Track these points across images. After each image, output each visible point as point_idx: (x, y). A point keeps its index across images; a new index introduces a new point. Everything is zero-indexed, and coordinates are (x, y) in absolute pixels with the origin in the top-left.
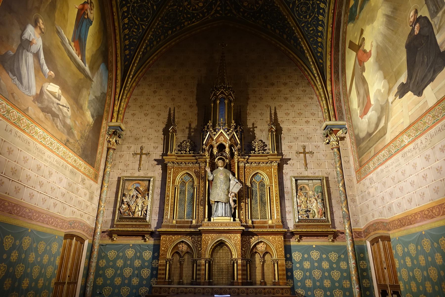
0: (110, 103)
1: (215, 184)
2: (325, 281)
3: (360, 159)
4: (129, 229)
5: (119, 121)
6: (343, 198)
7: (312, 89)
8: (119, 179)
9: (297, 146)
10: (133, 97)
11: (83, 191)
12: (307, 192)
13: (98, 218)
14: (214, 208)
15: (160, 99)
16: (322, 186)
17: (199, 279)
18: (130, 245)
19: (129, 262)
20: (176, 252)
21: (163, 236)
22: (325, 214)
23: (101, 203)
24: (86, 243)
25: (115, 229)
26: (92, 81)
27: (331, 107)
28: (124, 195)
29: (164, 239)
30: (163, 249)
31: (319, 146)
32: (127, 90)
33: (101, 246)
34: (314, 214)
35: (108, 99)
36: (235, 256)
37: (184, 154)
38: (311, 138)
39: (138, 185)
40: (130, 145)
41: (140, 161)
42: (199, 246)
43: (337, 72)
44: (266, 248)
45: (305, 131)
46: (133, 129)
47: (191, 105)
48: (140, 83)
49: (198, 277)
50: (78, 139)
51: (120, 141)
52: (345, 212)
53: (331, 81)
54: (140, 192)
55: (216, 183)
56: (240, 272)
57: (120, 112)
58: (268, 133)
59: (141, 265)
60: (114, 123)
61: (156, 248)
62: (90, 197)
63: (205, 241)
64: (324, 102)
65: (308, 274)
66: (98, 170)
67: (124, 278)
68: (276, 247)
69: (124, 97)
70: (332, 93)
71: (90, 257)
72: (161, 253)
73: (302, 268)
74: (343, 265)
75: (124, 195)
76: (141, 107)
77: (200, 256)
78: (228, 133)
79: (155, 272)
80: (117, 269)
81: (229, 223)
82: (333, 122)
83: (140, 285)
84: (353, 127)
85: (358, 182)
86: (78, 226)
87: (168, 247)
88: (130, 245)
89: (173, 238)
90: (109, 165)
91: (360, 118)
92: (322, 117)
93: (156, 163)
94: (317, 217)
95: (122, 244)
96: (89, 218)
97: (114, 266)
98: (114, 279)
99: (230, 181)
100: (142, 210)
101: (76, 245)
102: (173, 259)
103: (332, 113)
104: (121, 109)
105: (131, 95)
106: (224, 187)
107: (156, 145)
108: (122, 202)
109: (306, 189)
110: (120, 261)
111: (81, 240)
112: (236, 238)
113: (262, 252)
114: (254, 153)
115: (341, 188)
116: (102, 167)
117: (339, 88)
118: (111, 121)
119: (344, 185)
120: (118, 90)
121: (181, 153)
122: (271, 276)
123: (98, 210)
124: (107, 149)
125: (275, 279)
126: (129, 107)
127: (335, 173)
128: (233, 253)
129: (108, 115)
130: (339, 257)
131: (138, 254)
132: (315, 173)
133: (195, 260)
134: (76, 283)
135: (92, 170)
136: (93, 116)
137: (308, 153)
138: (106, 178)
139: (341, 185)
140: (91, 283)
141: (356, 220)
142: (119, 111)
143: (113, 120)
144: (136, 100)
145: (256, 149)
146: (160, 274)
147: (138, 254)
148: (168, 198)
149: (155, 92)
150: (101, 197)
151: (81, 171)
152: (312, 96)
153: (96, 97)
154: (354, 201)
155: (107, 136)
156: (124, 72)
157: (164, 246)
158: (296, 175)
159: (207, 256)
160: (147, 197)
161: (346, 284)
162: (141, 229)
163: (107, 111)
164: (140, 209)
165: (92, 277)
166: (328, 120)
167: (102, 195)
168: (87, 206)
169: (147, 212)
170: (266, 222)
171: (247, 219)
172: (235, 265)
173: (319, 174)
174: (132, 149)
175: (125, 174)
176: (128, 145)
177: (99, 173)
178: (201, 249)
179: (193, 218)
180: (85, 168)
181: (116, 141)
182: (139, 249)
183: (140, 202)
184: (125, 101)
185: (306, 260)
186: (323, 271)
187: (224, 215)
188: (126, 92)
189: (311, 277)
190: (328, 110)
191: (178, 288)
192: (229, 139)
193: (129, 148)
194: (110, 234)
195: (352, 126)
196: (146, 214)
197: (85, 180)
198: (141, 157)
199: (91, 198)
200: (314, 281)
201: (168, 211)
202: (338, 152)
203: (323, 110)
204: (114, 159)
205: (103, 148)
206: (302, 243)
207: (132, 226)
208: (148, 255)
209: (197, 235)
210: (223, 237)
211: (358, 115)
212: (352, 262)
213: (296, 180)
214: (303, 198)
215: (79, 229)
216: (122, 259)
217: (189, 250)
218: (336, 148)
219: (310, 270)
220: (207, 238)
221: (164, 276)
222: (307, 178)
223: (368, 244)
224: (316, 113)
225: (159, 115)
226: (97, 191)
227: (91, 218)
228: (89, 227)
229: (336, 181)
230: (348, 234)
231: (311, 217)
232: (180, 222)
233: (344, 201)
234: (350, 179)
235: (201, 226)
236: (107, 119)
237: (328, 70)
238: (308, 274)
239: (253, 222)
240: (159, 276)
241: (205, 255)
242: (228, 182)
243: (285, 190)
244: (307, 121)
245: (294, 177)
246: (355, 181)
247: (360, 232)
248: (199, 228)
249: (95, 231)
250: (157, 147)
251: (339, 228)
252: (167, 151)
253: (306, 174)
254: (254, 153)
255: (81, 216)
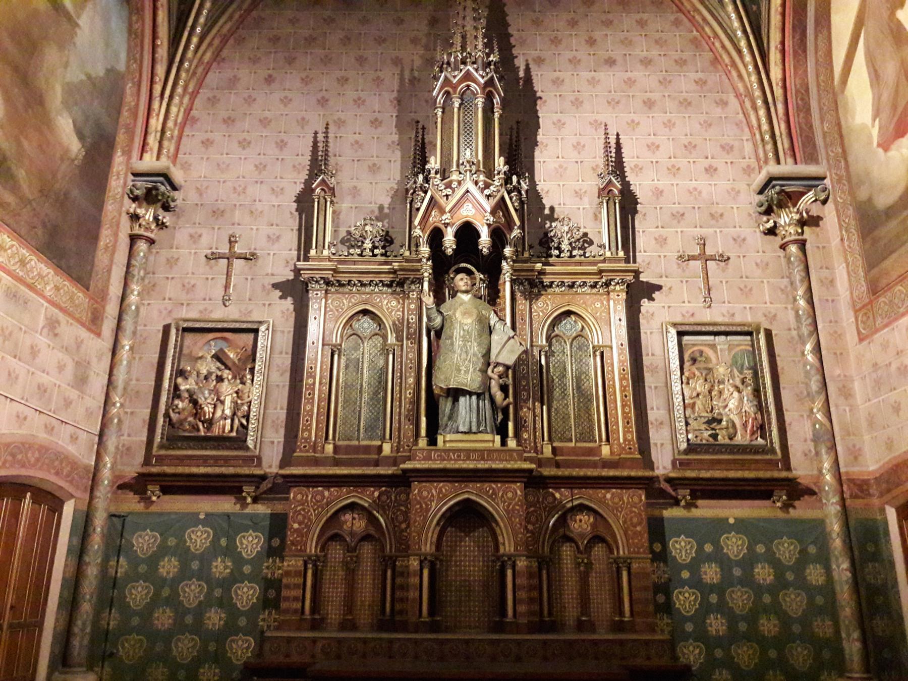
0: (137, 105)
1: (448, 342)
2: (763, 621)
3: (875, 271)
4: (195, 470)
5: (164, 159)
6: (815, 386)
7: (724, 77)
8: (166, 329)
9: (681, 239)
10: (204, 93)
11: (50, 356)
12: (710, 366)
13: (105, 438)
14: (445, 406)
15: (286, 101)
16: (754, 351)
17: (401, 612)
18: (198, 514)
19: (195, 565)
20: (331, 533)
21: (295, 489)
22: (762, 429)
23: (112, 394)
24: (68, 509)
25: (155, 470)
26: (77, 25)
27: (783, 126)
28: (181, 373)
29: (299, 497)
30: (296, 526)
31: (744, 240)
32: (187, 71)
33: (114, 518)
34: (731, 430)
35: (128, 91)
36: (507, 546)
37: (356, 258)
38: (722, 215)
39: (222, 344)
40: (199, 231)
41: (228, 275)
42: (401, 518)
43: (800, 27)
44: (594, 526)
45: (704, 194)
46: (205, 184)
47: (376, 120)
48: (225, 53)
49: (398, 607)
50: (31, 197)
51: (167, 218)
52: (821, 424)
53: (783, 52)
54: (230, 364)
55: (451, 337)
56: (522, 595)
57: (168, 134)
58: (597, 201)
59: (232, 572)
60: (149, 162)
61: (277, 526)
62: (75, 376)
63: (419, 503)
64: (762, 112)
65: (714, 598)
66: (102, 297)
67: (180, 611)
68: (625, 522)
69: (179, 90)
70: (785, 87)
71: (79, 551)
72: (290, 537)
73: (697, 583)
74: (815, 575)
75: (181, 373)
76: (229, 121)
77: (404, 547)
78: (487, 192)
79: (272, 594)
80: (159, 583)
81: (490, 451)
82: (787, 167)
83: (230, 629)
84: (849, 181)
85: (861, 340)
86: (38, 460)
87: (310, 520)
88: (198, 514)
89: (326, 493)
90: (135, 288)
91: (880, 150)
92: (753, 157)
93: (278, 293)
94: (741, 438)
95: (176, 513)
96: (74, 439)
97: (151, 576)
98: (151, 614)
99: (491, 332)
100: (234, 414)
101: (34, 517)
102: (325, 556)
103: (783, 144)
104: (170, 124)
105: (200, 84)
106: (475, 349)
107: (274, 230)
108: (176, 392)
109: (708, 360)
110: (169, 561)
111: (51, 501)
112: (510, 495)
113: (582, 536)
114: (558, 256)
115: (810, 358)
116: (115, 290)
117: (806, 71)
118: (141, 159)
119: (818, 349)
120: (161, 70)
121: (349, 254)
122: (607, 607)
123: (104, 416)
124: (128, 241)
125: (622, 613)
126: (195, 120)
127: (791, 314)
128: (500, 539)
129: (132, 140)
130: (803, 552)
131: (223, 542)
132: (733, 315)
133: (390, 558)
134: (40, 625)
135: (80, 296)
136: (81, 136)
137: (712, 258)
138: (128, 323)
139: (809, 347)
140: (84, 624)
141: (854, 446)
142: (163, 132)
143: (147, 156)
144: (213, 101)
145: (565, 246)
146: (287, 599)
147: (223, 542)
148: (310, 381)
149: (269, 80)
150: (114, 378)
151: (44, 297)
152: (724, 97)
153: (89, 77)
154: (846, 393)
155: (127, 200)
156: (179, 20)
157: (300, 518)
158: (678, 319)
159: (428, 548)
160: (249, 377)
161: (823, 627)
162: (231, 470)
163: (127, 126)
164: (228, 412)
165: (86, 608)
166: (772, 162)
167: (115, 372)
168: (68, 403)
169: (248, 421)
170: (596, 451)
171: (539, 440)
172: (509, 573)
173: (744, 317)
174: (205, 240)
175: (184, 313)
176: (192, 231)
177: (104, 307)
178: (408, 526)
179: (383, 439)
180: (57, 288)
181: (156, 219)
182: (229, 527)
183: (227, 390)
184: (181, 103)
185: (709, 558)
186: (758, 590)
187: (474, 429)
188: (183, 75)
189: (722, 608)
190: (773, 136)
191: (339, 641)
192: (489, 209)
193: (195, 238)
194: (138, 485)
195: (849, 180)
196: (245, 428)
197: (58, 322)
198: (229, 265)
199: (81, 381)
200: (732, 619)
201: (311, 417)
202: (801, 254)
203: (758, 136)
204: (150, 269)
205: (116, 235)
206: (696, 513)
207: (205, 460)
208: (251, 543)
209: (396, 487)
210: (471, 492)
211: (871, 143)
212: (842, 569)
213: (680, 334)
214: (699, 386)
215: (40, 469)
216: (174, 554)
217: (372, 531)
218: (795, 242)
219: (720, 589)
220: (425, 494)
221: (299, 605)
222: (711, 329)
223: (892, 515)
224: (736, 144)
225: (282, 145)
226: (100, 359)
227: (83, 436)
228: (74, 465)
229: (792, 338)
230: (830, 486)
231: (722, 439)
232: (349, 449)
233: (818, 393)
234: (836, 332)
235: (409, 458)
236: (128, 153)
237: (776, 19)
238: (714, 598)
239: (554, 450)
240: (284, 605)
241: (419, 543)
242: (485, 336)
243: (646, 361)
244: (710, 167)
245: (675, 325)
246: (851, 337)
247: (866, 482)
248: (402, 466)
249: (95, 475)
250: (278, 237)
251: (801, 469)
252: (307, 251)
253: (707, 316)
254: (558, 256)
255: (50, 429)
